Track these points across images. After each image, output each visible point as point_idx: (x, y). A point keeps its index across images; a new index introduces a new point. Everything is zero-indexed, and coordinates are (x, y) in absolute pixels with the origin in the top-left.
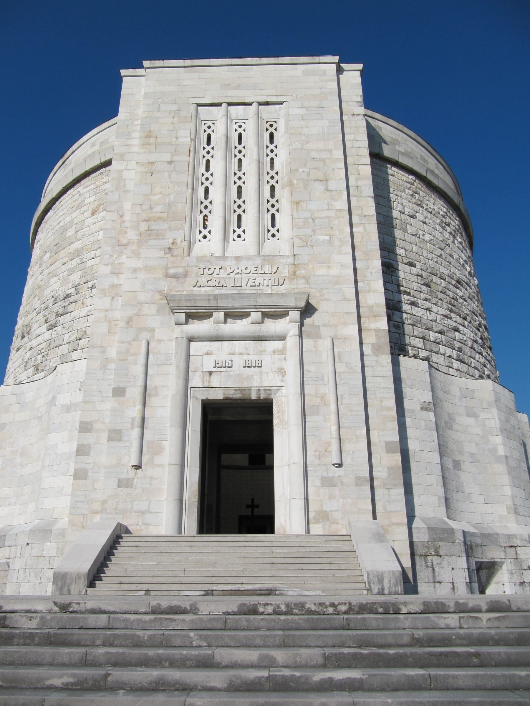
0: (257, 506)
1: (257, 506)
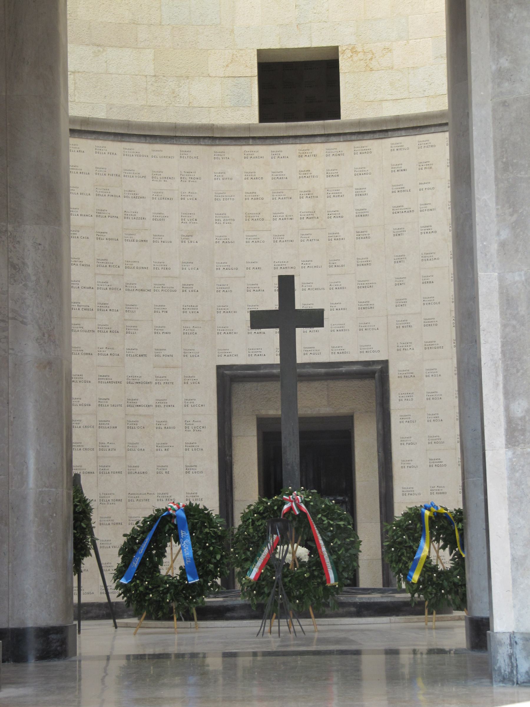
0: (315, 318)
1: (315, 318)
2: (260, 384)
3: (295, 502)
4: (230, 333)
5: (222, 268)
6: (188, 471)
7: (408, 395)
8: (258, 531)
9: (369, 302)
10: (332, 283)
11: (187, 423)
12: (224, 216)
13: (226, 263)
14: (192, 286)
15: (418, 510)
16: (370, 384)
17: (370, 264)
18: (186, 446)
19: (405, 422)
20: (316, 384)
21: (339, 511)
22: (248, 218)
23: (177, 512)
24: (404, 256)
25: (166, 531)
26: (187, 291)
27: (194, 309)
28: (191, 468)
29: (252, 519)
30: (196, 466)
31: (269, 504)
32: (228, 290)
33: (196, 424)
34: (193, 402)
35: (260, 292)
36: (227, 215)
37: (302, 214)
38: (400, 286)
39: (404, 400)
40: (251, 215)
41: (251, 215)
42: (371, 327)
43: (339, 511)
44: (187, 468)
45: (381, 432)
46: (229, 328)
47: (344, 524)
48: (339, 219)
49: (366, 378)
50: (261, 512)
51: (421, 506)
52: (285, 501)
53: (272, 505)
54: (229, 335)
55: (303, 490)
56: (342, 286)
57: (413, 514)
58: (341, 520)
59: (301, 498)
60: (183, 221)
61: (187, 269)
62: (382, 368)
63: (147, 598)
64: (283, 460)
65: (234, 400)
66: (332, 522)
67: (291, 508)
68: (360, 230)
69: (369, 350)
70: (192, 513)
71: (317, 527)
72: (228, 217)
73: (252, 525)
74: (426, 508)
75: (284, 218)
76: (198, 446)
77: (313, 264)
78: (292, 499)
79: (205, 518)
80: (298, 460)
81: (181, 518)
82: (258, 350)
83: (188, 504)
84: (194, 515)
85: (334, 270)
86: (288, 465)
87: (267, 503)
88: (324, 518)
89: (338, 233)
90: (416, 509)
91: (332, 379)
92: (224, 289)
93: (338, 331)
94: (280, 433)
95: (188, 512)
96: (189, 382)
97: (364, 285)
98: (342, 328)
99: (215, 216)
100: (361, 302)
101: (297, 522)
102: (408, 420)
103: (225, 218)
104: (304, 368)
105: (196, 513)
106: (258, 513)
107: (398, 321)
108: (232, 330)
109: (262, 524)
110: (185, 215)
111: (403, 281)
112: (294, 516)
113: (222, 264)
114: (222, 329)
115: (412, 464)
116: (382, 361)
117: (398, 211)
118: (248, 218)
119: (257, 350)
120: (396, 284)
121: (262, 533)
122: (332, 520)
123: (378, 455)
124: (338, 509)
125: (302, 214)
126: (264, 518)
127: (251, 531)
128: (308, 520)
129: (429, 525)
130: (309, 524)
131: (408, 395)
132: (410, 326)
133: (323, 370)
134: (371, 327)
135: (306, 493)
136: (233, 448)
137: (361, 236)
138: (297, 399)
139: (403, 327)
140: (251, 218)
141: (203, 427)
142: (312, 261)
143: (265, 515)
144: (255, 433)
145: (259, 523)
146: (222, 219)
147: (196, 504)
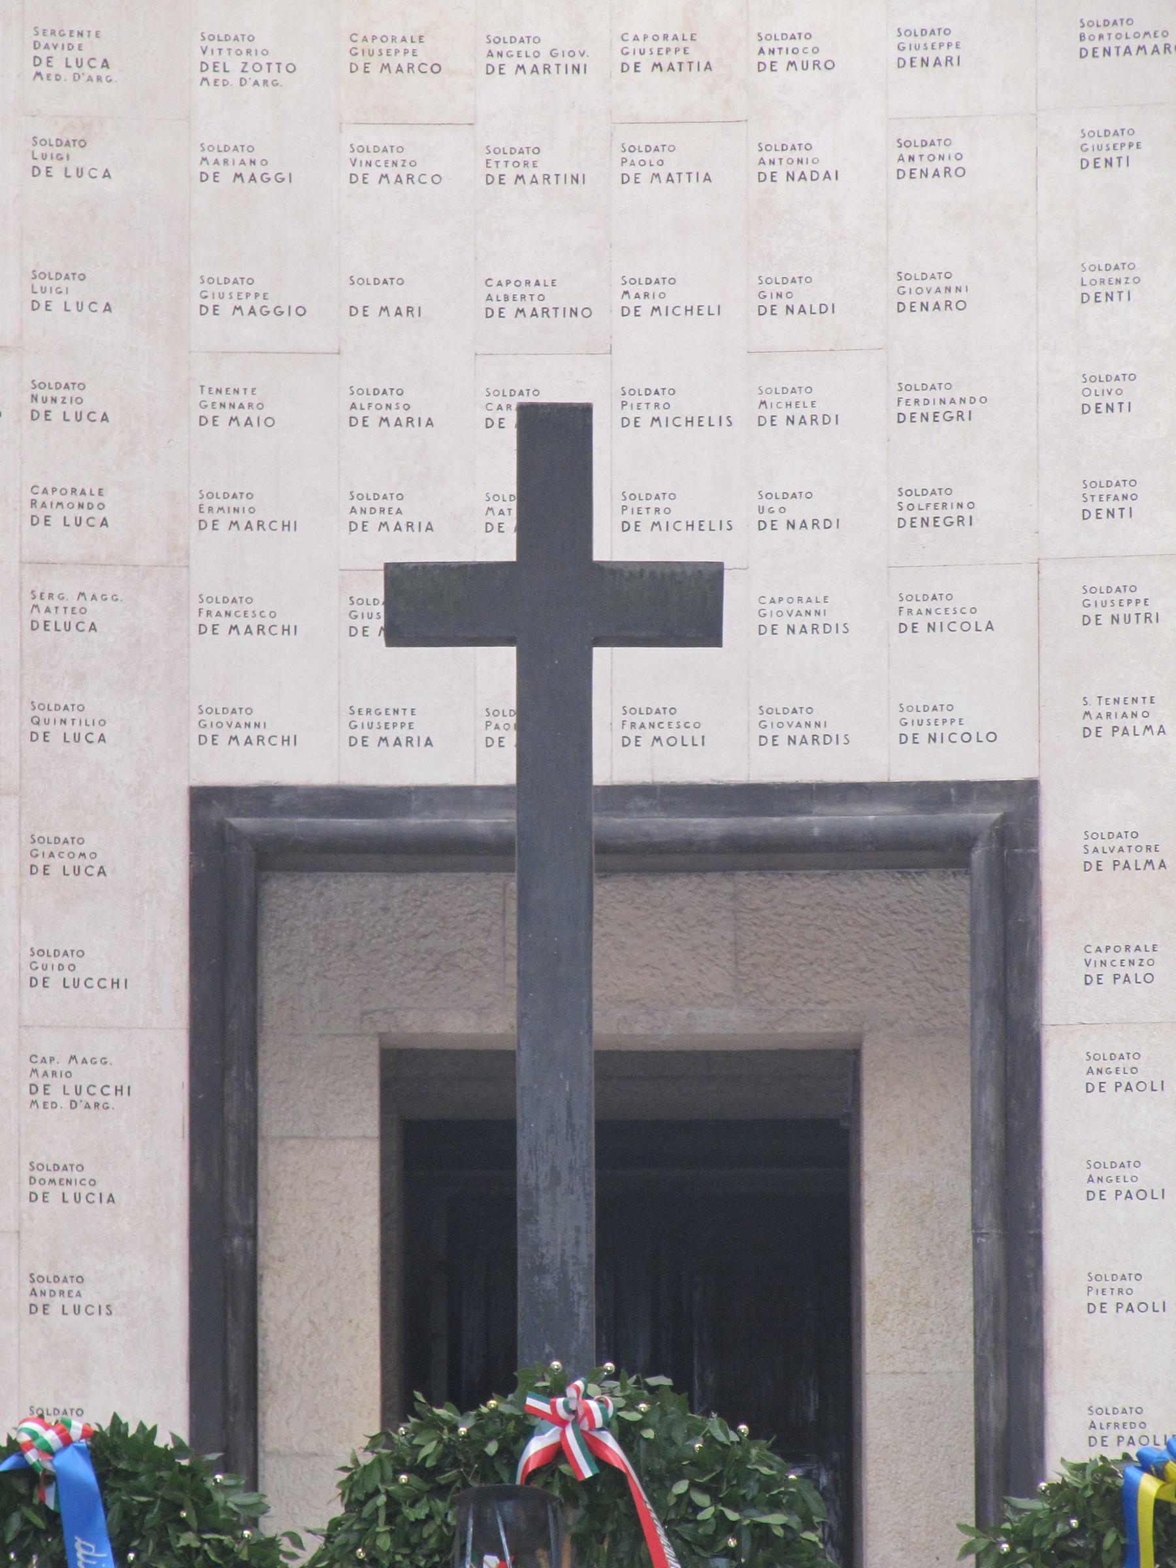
0: (681, 606)
1: (681, 606)
2: (400, 883)
3: (577, 1423)
4: (260, 629)
5: (226, 306)
6: (39, 1301)
7: (1132, 955)
8: (414, 1548)
9: (949, 491)
10: (769, 391)
11: (41, 1068)
12: (244, 45)
13: (251, 282)
14: (76, 392)
15: (1113, 1474)
16: (945, 902)
17: (962, 305)
18: (32, 1180)
19: (1109, 1087)
20: (680, 890)
21: (765, 1470)
22: (360, 60)
23: (59, 1461)
24: (1131, 266)
25: (10, 1537)
26: (56, 415)
27: (85, 507)
28: (57, 1287)
29: (387, 1493)
30: (80, 1279)
31: (463, 1430)
32: (254, 414)
33: (84, 1075)
34: (72, 968)
35: (415, 430)
36: (258, 45)
37: (632, 45)
38: (1106, 416)
39: (1107, 979)
40: (377, 45)
41: (377, 45)
42: (960, 618)
43: (765, 1470)
44: (38, 1287)
45: (994, 1135)
46: (256, 606)
47: (784, 1526)
48: (813, 77)
49: (922, 867)
50: (429, 1464)
51: (1126, 1457)
52: (536, 1421)
53: (477, 1435)
54: (255, 638)
55: (614, 1376)
56: (819, 410)
57: (1089, 1493)
58: (774, 1505)
59: (604, 1411)
60: (43, 69)
61: (57, 306)
62: (1004, 818)
63: (239, 1534)
64: (521, 1249)
65: (270, 959)
66: (732, 1516)
67: (559, 1452)
68: (916, 133)
69: (947, 729)
70: (122, 1465)
71: (668, 1534)
72: (265, 52)
73: (390, 1519)
74: (1145, 1465)
75: (540, 64)
76: (93, 1182)
77: (675, 296)
78: (562, 1413)
79: (181, 1488)
80: (587, 1248)
81: (77, 1485)
82: (399, 718)
83: (106, 1425)
84: (135, 1475)
85: (779, 330)
86: (542, 1270)
87: (454, 1428)
88: (701, 1499)
89: (809, 147)
90: (1105, 1469)
91: (761, 869)
92: (236, 408)
93: (791, 629)
94: (507, 1129)
95: (107, 1462)
96: (56, 865)
97: (930, 409)
98: (812, 619)
99: (198, 44)
100: (910, 492)
101: (581, 1512)
102: (1124, 1079)
103: (251, 60)
104: (623, 810)
105: (141, 1468)
106: (418, 1469)
107: (1094, 590)
108: (273, 615)
109: (430, 1517)
110: (51, 40)
111: (1119, 392)
112: (574, 1488)
113: (230, 287)
114: (222, 608)
115: (1141, 1292)
116: (1008, 785)
117: (1105, 43)
118: (360, 60)
119: (391, 719)
120: (1085, 409)
121: (429, 1556)
122: (735, 1509)
123: (976, 1246)
124: (761, 1462)
125: (632, 45)
126: (441, 1491)
127: (384, 1543)
128: (631, 1505)
129: (1157, 1537)
130: (638, 1523)
131: (1132, 955)
132: (1147, 617)
133: (713, 826)
134: (960, 618)
135: (624, 1387)
136: (261, 1196)
137: (918, 165)
138: (589, 973)
139: (1115, 619)
140: (375, 63)
141: (118, 1090)
142: (672, 281)
143: (442, 1479)
144: (371, 1124)
145: (421, 1512)
146: (235, 64)
147: (142, 1427)
